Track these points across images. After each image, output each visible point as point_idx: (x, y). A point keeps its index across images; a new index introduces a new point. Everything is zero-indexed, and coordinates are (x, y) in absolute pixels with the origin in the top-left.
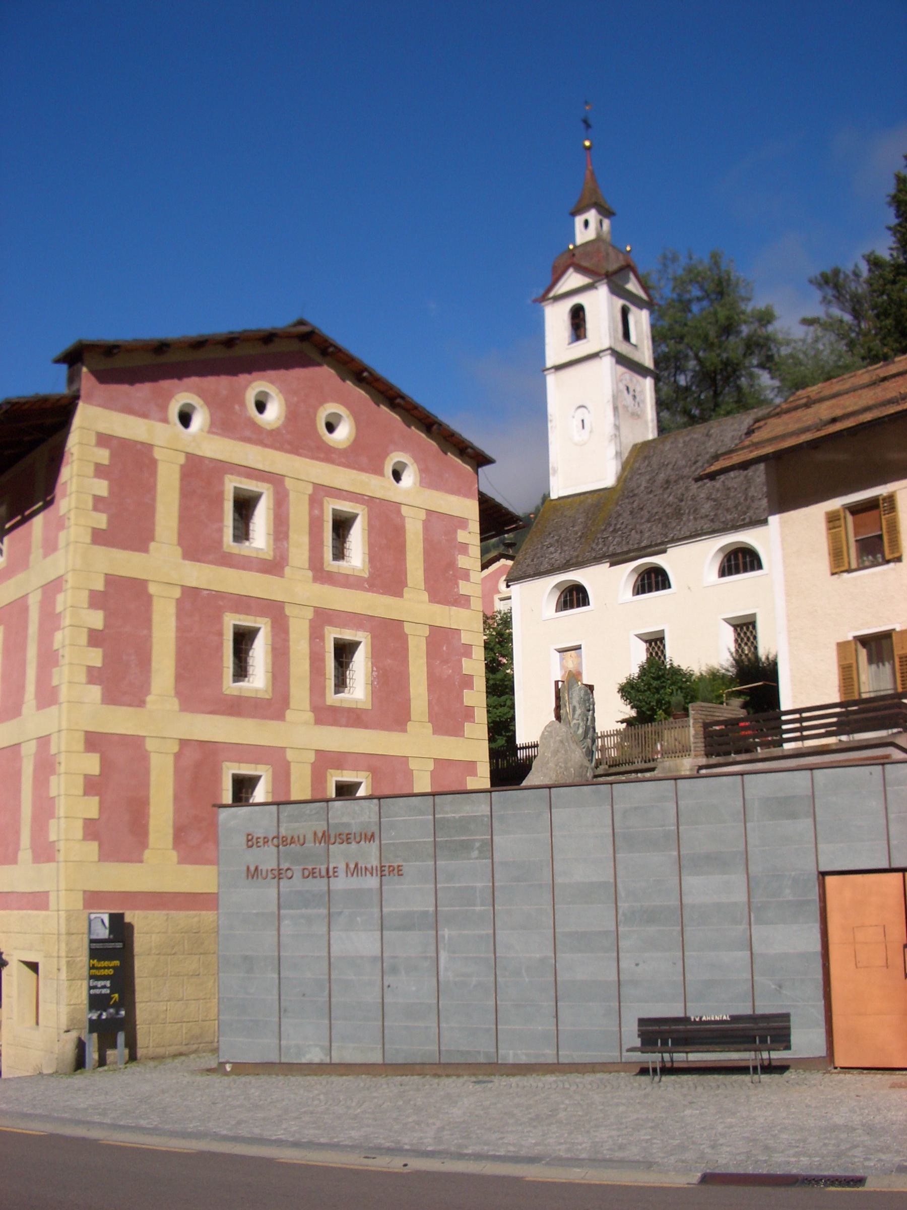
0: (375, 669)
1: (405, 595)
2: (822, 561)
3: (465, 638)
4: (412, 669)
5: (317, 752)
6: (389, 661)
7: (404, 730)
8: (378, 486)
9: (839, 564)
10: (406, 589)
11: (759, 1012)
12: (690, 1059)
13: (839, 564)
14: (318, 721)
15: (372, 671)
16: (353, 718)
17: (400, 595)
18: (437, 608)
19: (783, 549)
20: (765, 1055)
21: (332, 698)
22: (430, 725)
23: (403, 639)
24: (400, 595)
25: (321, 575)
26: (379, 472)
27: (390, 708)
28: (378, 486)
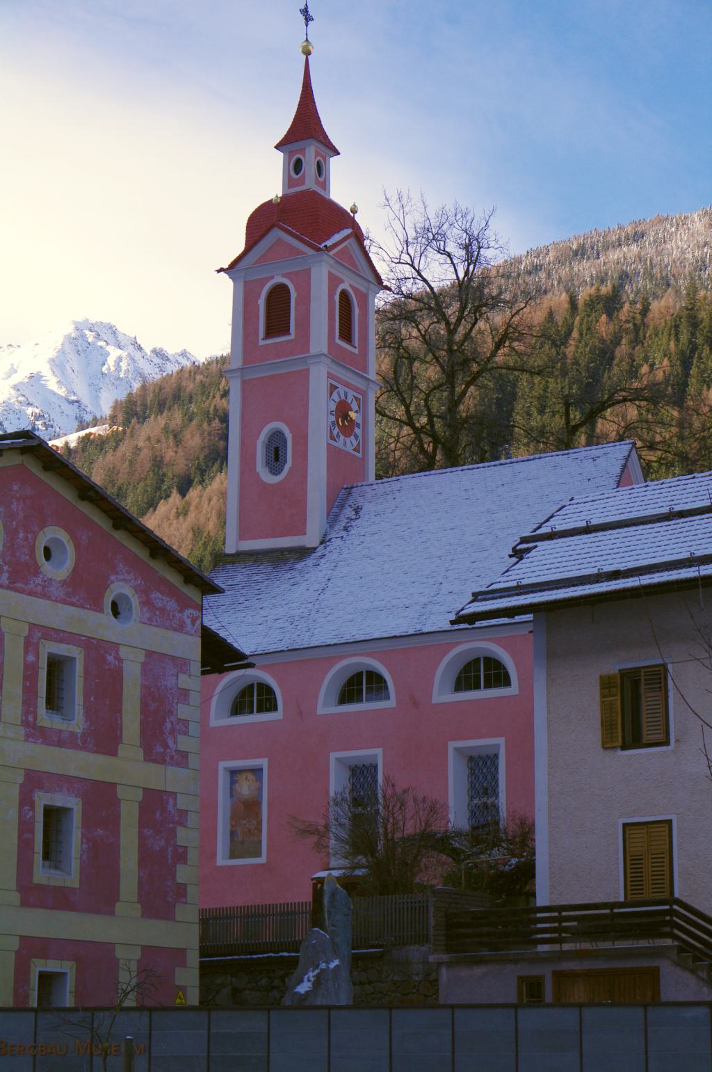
0: (85, 841)
1: (120, 753)
2: (593, 734)
3: (182, 803)
4: (123, 842)
5: (23, 938)
6: (100, 832)
7: (112, 913)
8: (100, 625)
9: (607, 744)
10: (121, 746)
11: (66, 886)
12: (564, 949)
13: (607, 744)
14: (25, 903)
15: (82, 843)
16: (59, 899)
17: (114, 753)
18: (153, 767)
19: (549, 712)
20: (90, 515)
21: (42, 874)
22: (139, 906)
23: (115, 802)
24: (114, 753)
25: (34, 732)
26: (97, 606)
27: (99, 893)
28: (100, 625)
